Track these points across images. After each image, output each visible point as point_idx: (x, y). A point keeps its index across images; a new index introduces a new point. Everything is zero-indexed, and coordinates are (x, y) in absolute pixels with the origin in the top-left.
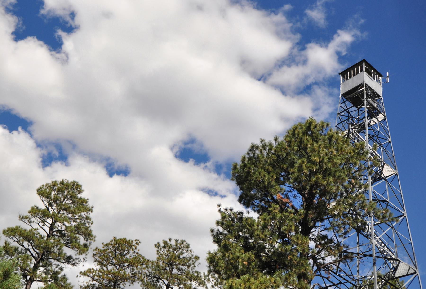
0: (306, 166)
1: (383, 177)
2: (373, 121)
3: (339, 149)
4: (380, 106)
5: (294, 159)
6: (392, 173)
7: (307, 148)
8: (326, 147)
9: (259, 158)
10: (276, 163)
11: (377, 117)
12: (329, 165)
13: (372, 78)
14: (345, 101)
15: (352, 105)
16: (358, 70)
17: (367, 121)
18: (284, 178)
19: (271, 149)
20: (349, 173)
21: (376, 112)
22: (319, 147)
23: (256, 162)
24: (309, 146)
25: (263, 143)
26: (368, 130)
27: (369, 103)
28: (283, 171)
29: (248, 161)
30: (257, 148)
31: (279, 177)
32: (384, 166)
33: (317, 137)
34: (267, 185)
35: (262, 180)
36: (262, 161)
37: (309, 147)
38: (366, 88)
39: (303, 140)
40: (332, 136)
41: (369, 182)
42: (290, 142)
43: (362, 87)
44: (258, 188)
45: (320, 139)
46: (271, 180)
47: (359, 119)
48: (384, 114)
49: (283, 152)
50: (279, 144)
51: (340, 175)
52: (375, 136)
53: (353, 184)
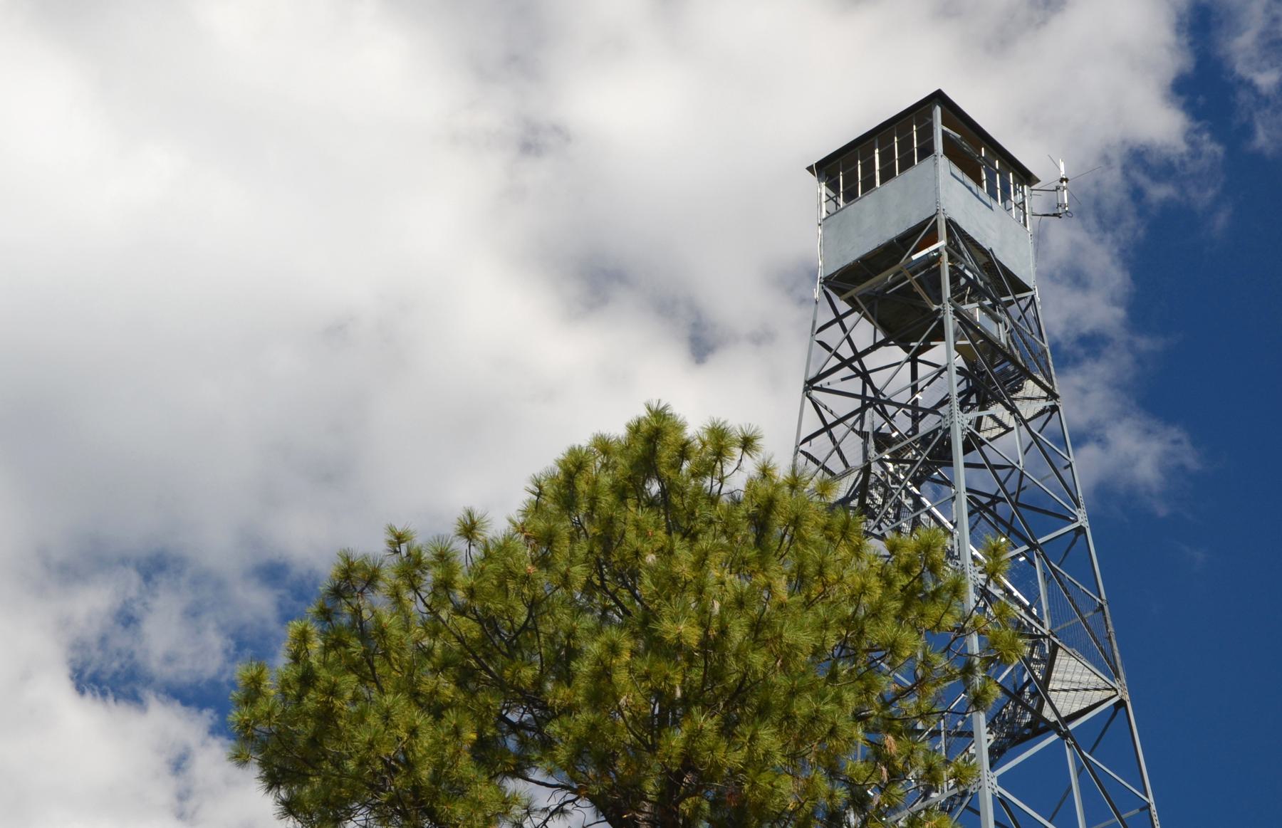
0: (631, 671)
1: (1053, 718)
2: (993, 417)
3: (811, 570)
4: (1027, 338)
5: (571, 635)
6: (1097, 696)
7: (635, 575)
8: (738, 565)
9: (382, 632)
10: (478, 660)
11: (1014, 396)
12: (758, 659)
13: (983, 193)
14: (841, 313)
15: (880, 337)
16: (906, 145)
17: (960, 422)
18: (523, 743)
19: (445, 585)
20: (864, 698)
21: (1004, 372)
22: (701, 563)
23: (368, 655)
24: (651, 558)
25: (404, 553)
26: (967, 465)
27: (966, 323)
28: (519, 702)
29: (326, 650)
30: (372, 579)
31: (494, 737)
32: (1057, 662)
33: (693, 513)
34: (427, 784)
35: (405, 752)
36: (403, 649)
37: (649, 569)
38: (952, 245)
39: (619, 527)
40: (769, 505)
41: (979, 748)
42: (549, 539)
43: (932, 238)
44: (384, 797)
45: (711, 522)
46: (450, 750)
47: (922, 409)
48: (1045, 382)
49: (512, 595)
50: (488, 556)
51: (817, 711)
52: (1003, 500)
53: (889, 762)
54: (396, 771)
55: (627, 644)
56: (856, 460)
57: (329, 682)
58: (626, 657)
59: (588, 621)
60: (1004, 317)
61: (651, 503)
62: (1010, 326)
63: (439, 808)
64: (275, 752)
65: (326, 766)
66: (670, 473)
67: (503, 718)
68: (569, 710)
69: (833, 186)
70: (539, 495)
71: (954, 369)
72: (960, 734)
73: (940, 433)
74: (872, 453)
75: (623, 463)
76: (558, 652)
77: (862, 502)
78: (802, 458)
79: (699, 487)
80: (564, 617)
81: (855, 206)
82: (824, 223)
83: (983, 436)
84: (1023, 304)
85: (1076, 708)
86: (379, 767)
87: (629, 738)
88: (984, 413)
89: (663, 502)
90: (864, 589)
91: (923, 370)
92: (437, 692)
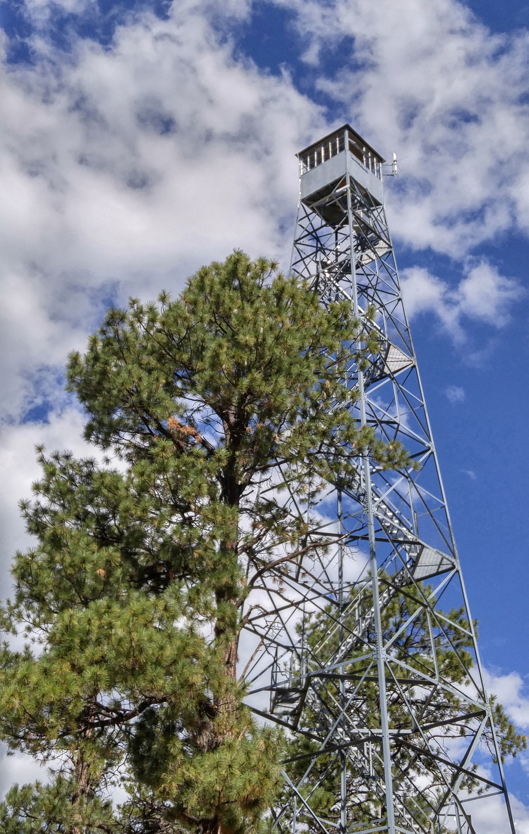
0: (227, 355)
1: (388, 372)
2: (367, 255)
3: (299, 316)
5: (203, 341)
7: (229, 317)
9: (127, 339)
12: (277, 351)
16: (334, 146)
22: (256, 313)
23: (121, 348)
24: (235, 311)
25: (136, 308)
27: (357, 218)
29: (104, 347)
38: (352, 187)
39: (222, 298)
40: (282, 290)
41: (360, 384)
42: (195, 303)
43: (344, 183)
44: (128, 405)
46: (154, 386)
50: (170, 309)
53: (327, 391)
54: (132, 395)
55: (226, 344)
56: (314, 272)
57: (105, 359)
58: (225, 349)
59: (210, 335)
60: (372, 215)
61: (235, 289)
62: (374, 219)
63: (150, 410)
64: (83, 387)
65: (104, 392)
66: (243, 277)
67: (175, 374)
68: (203, 370)
69: (305, 162)
70: (190, 285)
71: (352, 236)
72: (353, 379)
73: (347, 261)
74: (320, 269)
75: (223, 272)
76: (198, 348)
77: (316, 288)
78: (293, 271)
79: (254, 283)
80: (201, 334)
81: (314, 170)
82: (302, 177)
83: (363, 262)
84: (379, 210)
85: (397, 369)
86: (126, 393)
87: (226, 381)
88: (364, 254)
89: (240, 288)
90: (321, 324)
91: (340, 237)
92: (149, 364)
